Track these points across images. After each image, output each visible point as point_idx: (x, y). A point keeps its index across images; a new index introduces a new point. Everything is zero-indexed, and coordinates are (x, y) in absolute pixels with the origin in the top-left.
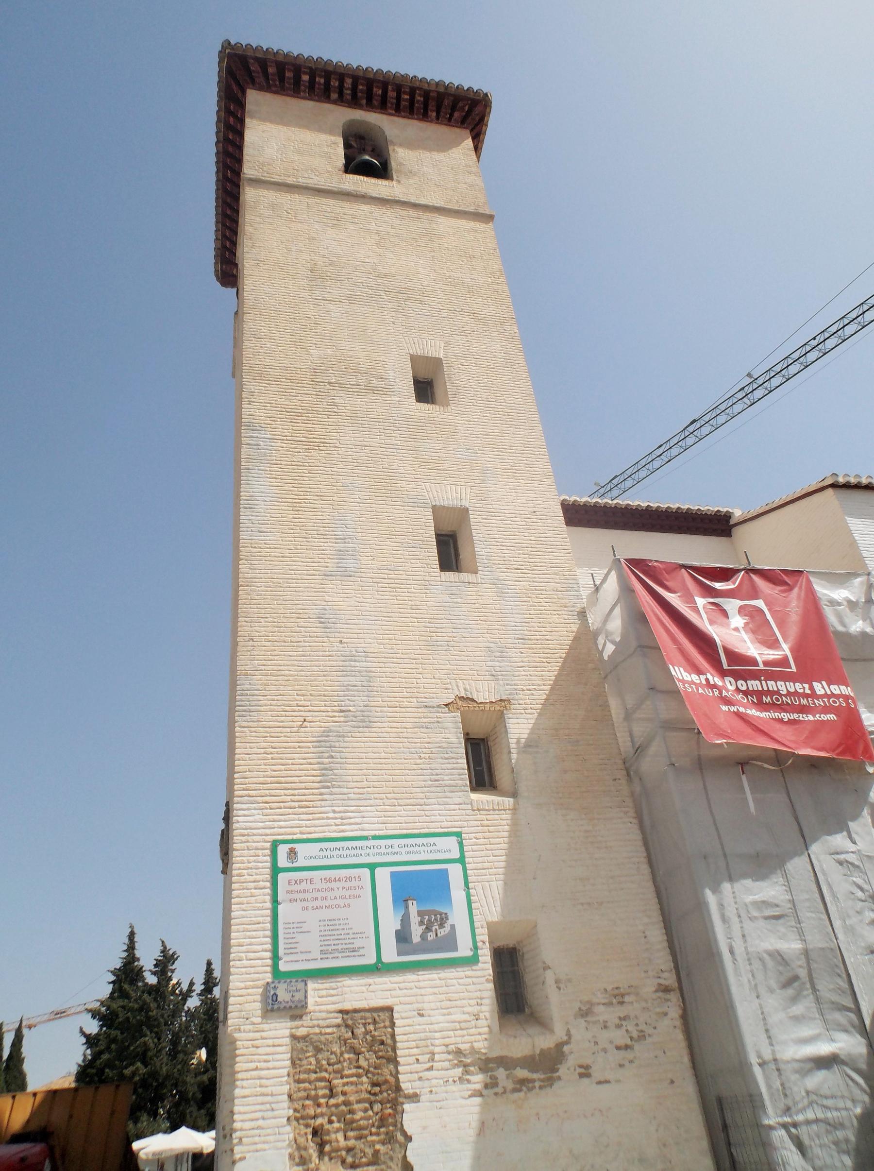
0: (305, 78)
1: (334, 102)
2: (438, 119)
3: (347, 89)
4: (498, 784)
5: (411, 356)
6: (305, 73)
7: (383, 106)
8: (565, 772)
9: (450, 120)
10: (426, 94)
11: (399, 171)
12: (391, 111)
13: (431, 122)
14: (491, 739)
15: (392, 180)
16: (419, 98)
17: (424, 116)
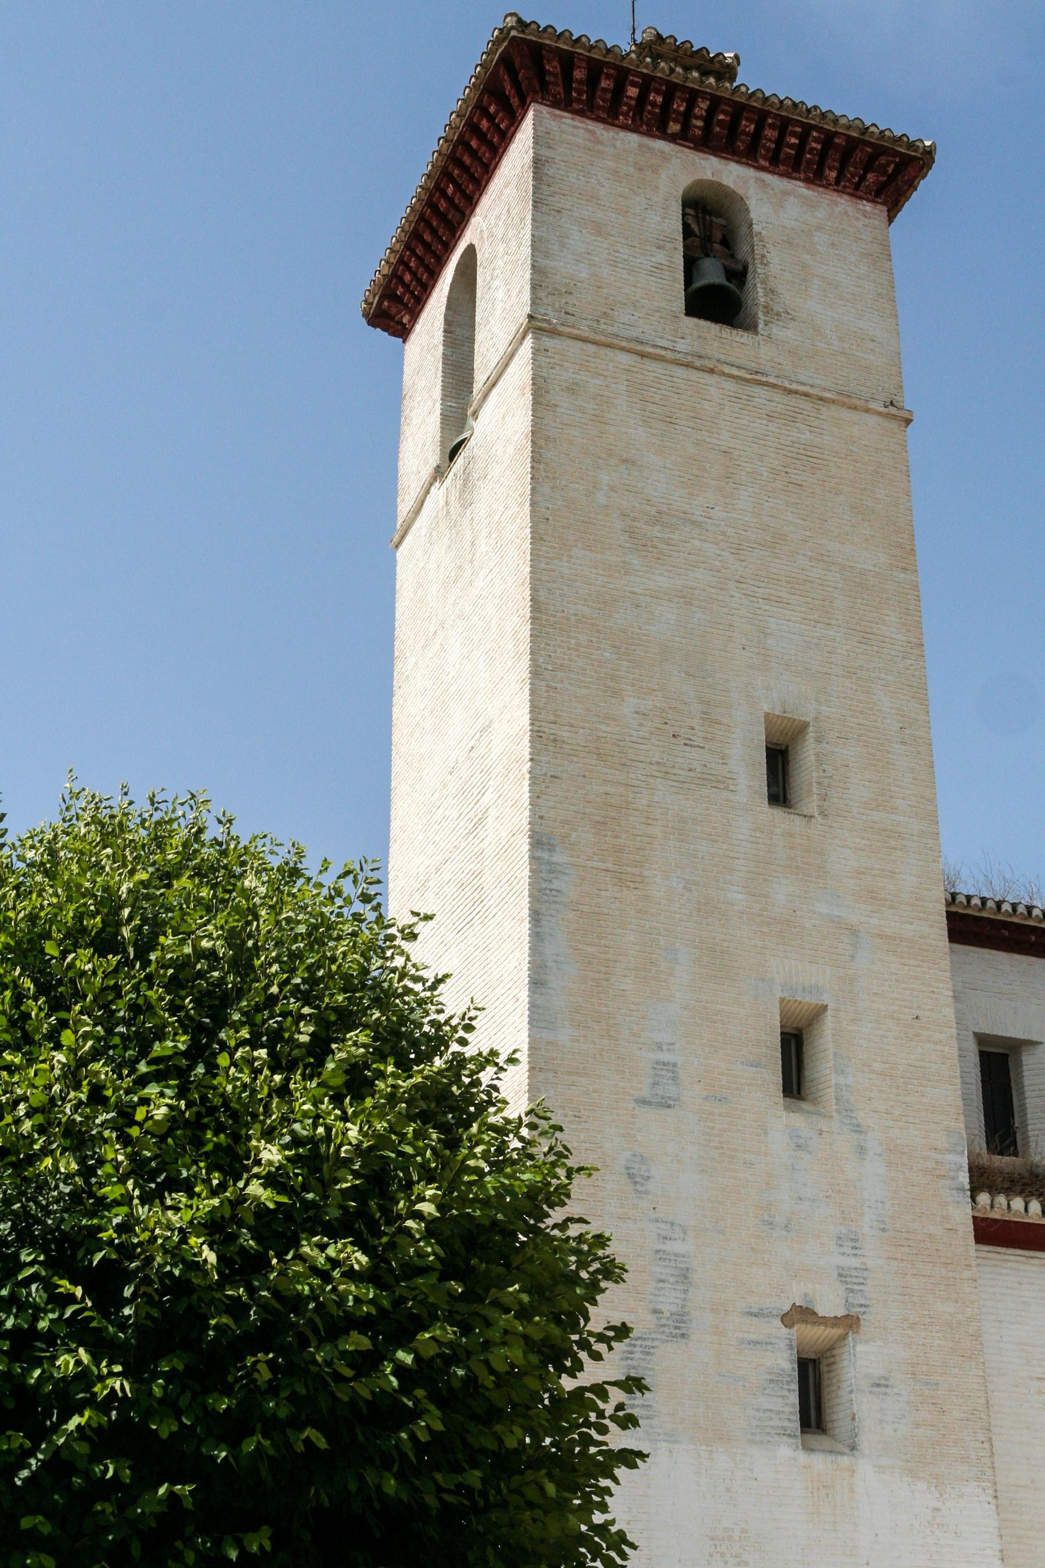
0: (633, 92)
1: (673, 138)
2: (838, 186)
3: (697, 118)
4: (829, 1426)
5: (975, 1034)
6: (634, 84)
7: (748, 153)
8: (917, 1426)
9: (857, 186)
10: (828, 139)
11: (768, 310)
12: (763, 162)
13: (826, 187)
14: (824, 1362)
15: (756, 333)
16: (814, 145)
17: (815, 178)
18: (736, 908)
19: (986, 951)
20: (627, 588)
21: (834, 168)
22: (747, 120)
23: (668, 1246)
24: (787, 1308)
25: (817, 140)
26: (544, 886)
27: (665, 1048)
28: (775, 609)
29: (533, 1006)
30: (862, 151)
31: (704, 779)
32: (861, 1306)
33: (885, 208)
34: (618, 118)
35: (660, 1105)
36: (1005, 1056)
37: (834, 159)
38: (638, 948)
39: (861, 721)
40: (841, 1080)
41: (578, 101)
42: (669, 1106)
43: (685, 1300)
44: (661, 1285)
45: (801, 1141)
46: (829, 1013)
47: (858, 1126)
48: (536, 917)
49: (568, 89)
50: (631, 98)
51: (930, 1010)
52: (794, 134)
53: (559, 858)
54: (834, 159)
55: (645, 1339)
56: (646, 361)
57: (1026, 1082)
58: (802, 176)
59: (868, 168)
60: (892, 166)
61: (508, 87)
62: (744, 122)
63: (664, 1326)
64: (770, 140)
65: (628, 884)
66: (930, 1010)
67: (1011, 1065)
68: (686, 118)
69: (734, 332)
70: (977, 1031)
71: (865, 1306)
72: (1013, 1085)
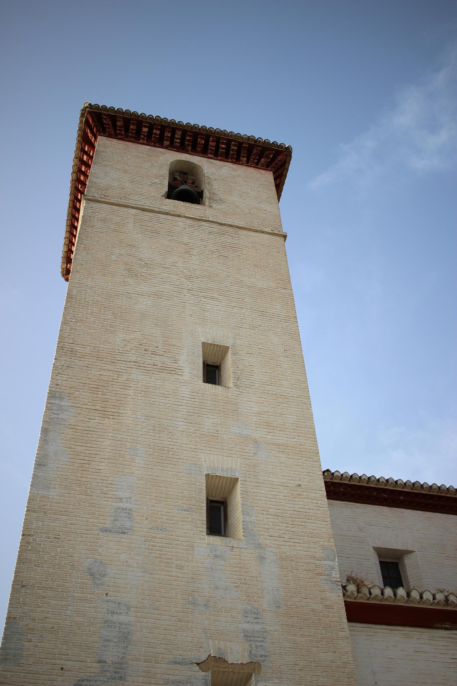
2: (248, 164)
5: (373, 547)
6: (145, 127)
12: (210, 156)
16: (233, 148)
17: (237, 160)
18: (179, 429)
19: (376, 506)
20: (124, 291)
21: (245, 157)
22: (200, 138)
23: (115, 618)
24: (204, 657)
25: (234, 145)
26: (53, 416)
27: (124, 500)
28: (210, 301)
29: (35, 477)
30: (256, 149)
31: (163, 369)
32: (261, 656)
33: (271, 173)
34: (140, 141)
35: (118, 532)
36: (397, 564)
37: (244, 153)
38: (111, 448)
39: (260, 347)
40: (248, 518)
41: (121, 135)
42: (124, 533)
43: (124, 653)
44: (107, 643)
45: (218, 553)
46: (239, 483)
47: (259, 544)
48: (45, 431)
49: (115, 130)
50: (145, 132)
51: (307, 482)
52: (223, 143)
53: (65, 403)
54: (244, 153)
55: (90, 680)
56: (145, 212)
57: (409, 573)
58: (230, 160)
59: (261, 156)
60: (272, 155)
61: (89, 135)
62: (199, 140)
63: (106, 671)
64: (212, 146)
65: (109, 416)
66: (307, 482)
67: (400, 568)
68: (172, 139)
69: (193, 205)
70: (375, 546)
71: (265, 656)
72: (403, 578)
